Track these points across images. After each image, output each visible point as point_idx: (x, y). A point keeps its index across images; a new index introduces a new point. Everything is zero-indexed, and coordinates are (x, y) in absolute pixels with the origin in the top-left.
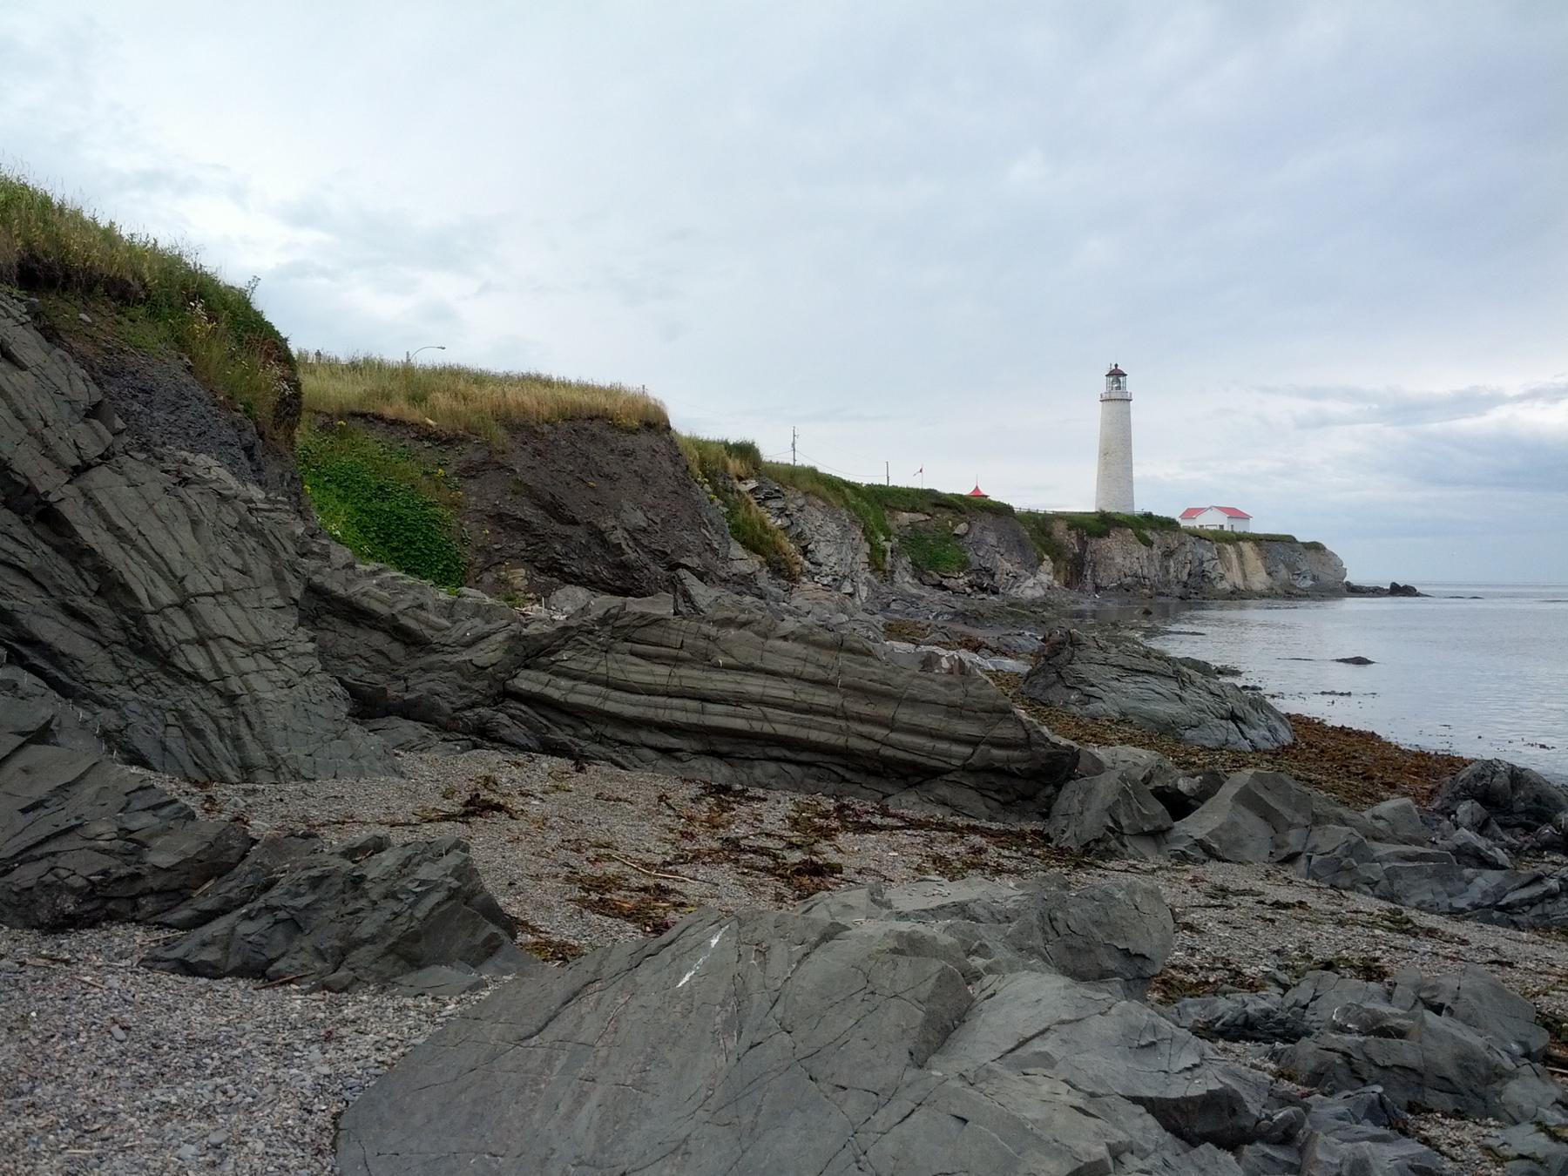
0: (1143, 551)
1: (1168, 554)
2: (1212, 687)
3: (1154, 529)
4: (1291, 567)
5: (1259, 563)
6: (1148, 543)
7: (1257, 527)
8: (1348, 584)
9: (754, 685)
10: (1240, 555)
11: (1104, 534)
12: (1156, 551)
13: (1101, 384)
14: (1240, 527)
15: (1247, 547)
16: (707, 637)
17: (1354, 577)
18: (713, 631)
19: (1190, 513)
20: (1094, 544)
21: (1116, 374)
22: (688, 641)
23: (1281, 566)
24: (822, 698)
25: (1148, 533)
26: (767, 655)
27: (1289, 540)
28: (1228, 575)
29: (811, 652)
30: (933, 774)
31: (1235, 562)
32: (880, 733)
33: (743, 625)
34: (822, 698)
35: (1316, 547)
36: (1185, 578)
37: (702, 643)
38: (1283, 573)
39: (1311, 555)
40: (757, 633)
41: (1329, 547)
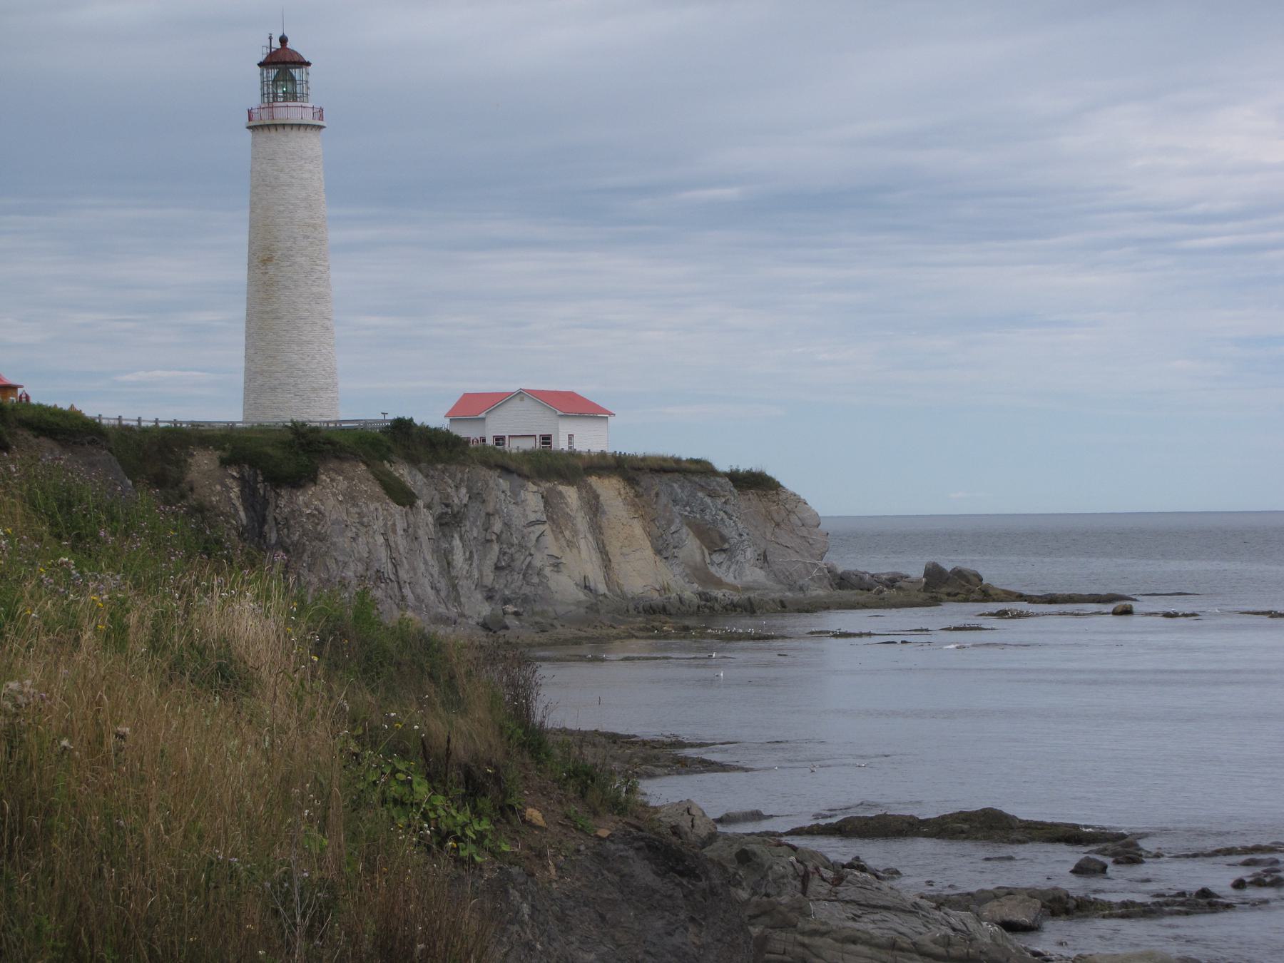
2: (953, 921)
3: (413, 461)
5: (638, 529)
6: (404, 497)
10: (594, 507)
11: (301, 478)
12: (426, 518)
14: (588, 439)
15: (609, 489)
16: (803, 945)
18: (806, 940)
19: (474, 405)
20: (285, 502)
21: (283, 64)
22: (789, 948)
25: (403, 472)
26: (846, 956)
27: (699, 471)
28: (568, 558)
29: (874, 951)
31: (582, 522)
33: (823, 934)
35: (755, 483)
37: (799, 950)
39: (749, 503)
40: (836, 940)
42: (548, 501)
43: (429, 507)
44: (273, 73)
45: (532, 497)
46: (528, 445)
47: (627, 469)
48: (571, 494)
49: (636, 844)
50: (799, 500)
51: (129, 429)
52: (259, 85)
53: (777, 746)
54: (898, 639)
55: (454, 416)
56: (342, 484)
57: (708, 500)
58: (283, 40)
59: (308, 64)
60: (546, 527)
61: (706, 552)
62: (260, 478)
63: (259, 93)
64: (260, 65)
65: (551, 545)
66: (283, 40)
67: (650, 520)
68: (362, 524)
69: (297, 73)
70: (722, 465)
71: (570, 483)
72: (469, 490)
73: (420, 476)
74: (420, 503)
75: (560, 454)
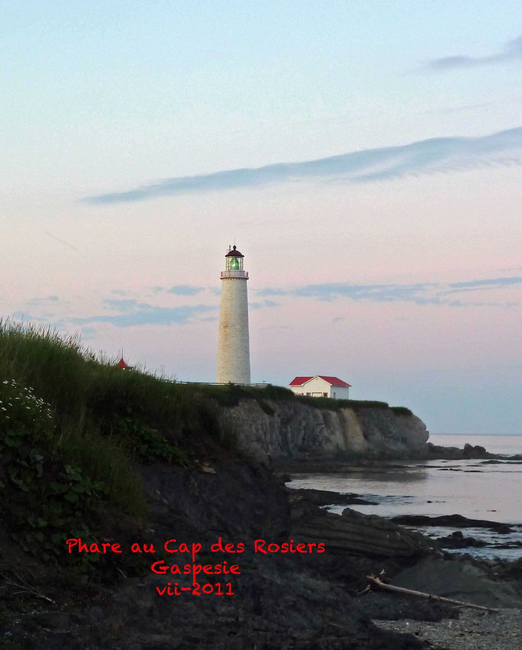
0: (267, 418)
1: (285, 422)
4: (385, 432)
6: (270, 412)
7: (354, 394)
8: (430, 445)
9: (341, 535)
10: (343, 421)
11: (233, 404)
12: (277, 419)
13: (222, 264)
14: (341, 395)
15: (348, 413)
17: (434, 440)
19: (299, 381)
21: (234, 254)
23: (376, 430)
24: (359, 538)
25: (269, 403)
27: (382, 406)
30: (387, 557)
32: (374, 547)
34: (359, 538)
35: (403, 412)
36: (300, 442)
38: (378, 436)
39: (400, 420)
41: (416, 412)
42: (325, 417)
43: (279, 416)
44: (230, 259)
45: (319, 412)
46: (319, 395)
47: (358, 407)
48: (334, 414)
49: (391, 435)
50: (418, 419)
51: (96, 363)
52: (225, 263)
53: (406, 500)
54: (449, 469)
55: (292, 384)
56: (247, 406)
57: (384, 418)
58: (235, 247)
59: (243, 256)
60: (323, 426)
61: (383, 437)
62: (217, 403)
63: (225, 266)
64: (226, 256)
65: (326, 433)
66: (235, 247)
67: (363, 424)
68: (254, 421)
69: (239, 260)
70: (391, 405)
71: (333, 410)
72: (294, 410)
73: (276, 405)
74: (276, 414)
75: (330, 399)
